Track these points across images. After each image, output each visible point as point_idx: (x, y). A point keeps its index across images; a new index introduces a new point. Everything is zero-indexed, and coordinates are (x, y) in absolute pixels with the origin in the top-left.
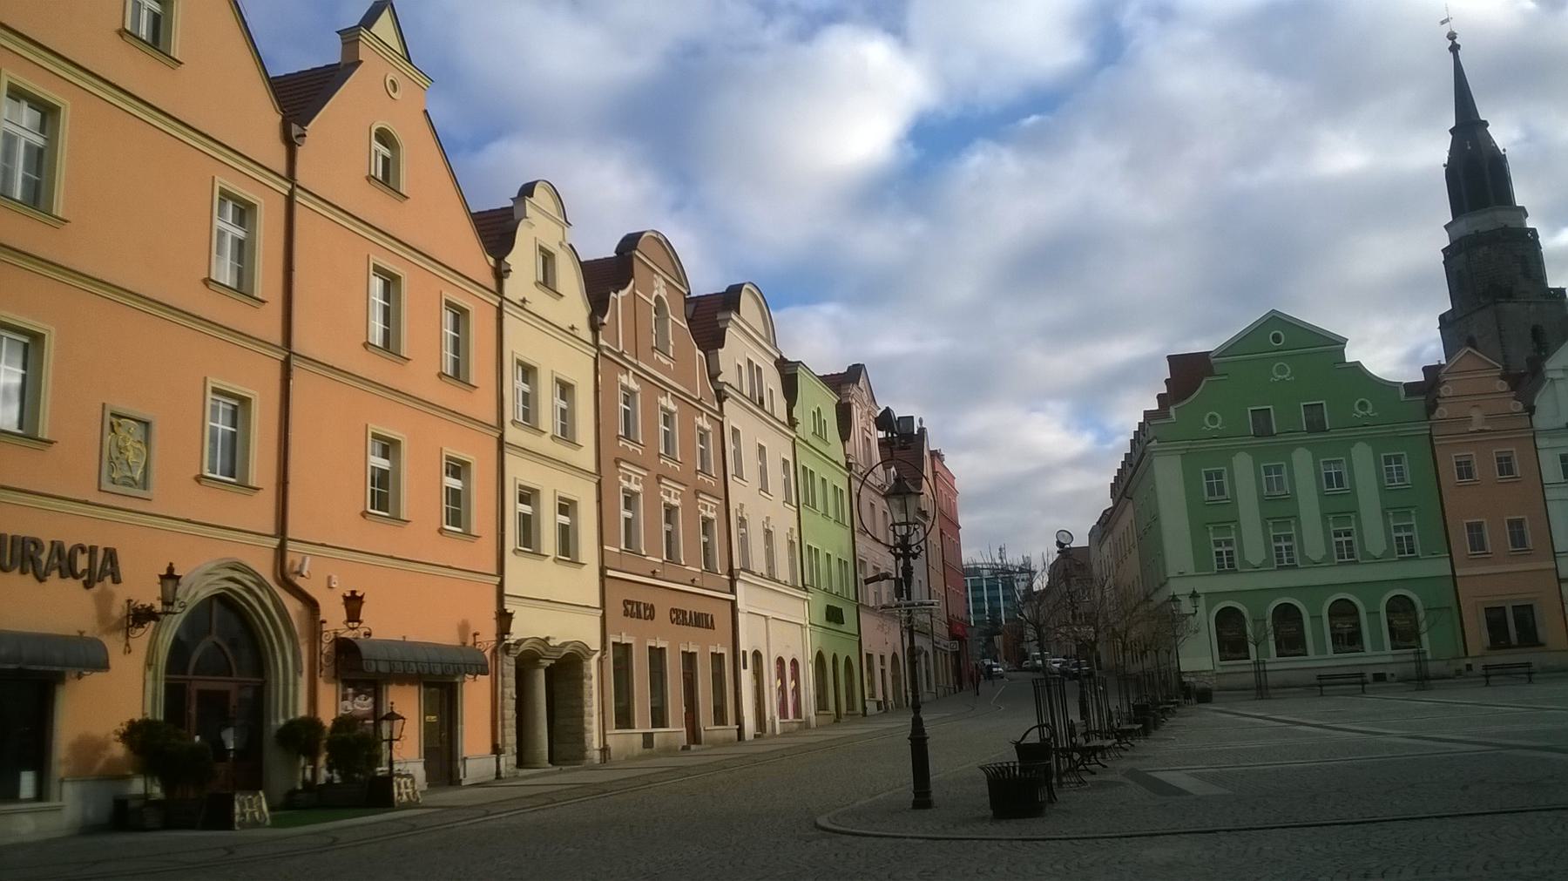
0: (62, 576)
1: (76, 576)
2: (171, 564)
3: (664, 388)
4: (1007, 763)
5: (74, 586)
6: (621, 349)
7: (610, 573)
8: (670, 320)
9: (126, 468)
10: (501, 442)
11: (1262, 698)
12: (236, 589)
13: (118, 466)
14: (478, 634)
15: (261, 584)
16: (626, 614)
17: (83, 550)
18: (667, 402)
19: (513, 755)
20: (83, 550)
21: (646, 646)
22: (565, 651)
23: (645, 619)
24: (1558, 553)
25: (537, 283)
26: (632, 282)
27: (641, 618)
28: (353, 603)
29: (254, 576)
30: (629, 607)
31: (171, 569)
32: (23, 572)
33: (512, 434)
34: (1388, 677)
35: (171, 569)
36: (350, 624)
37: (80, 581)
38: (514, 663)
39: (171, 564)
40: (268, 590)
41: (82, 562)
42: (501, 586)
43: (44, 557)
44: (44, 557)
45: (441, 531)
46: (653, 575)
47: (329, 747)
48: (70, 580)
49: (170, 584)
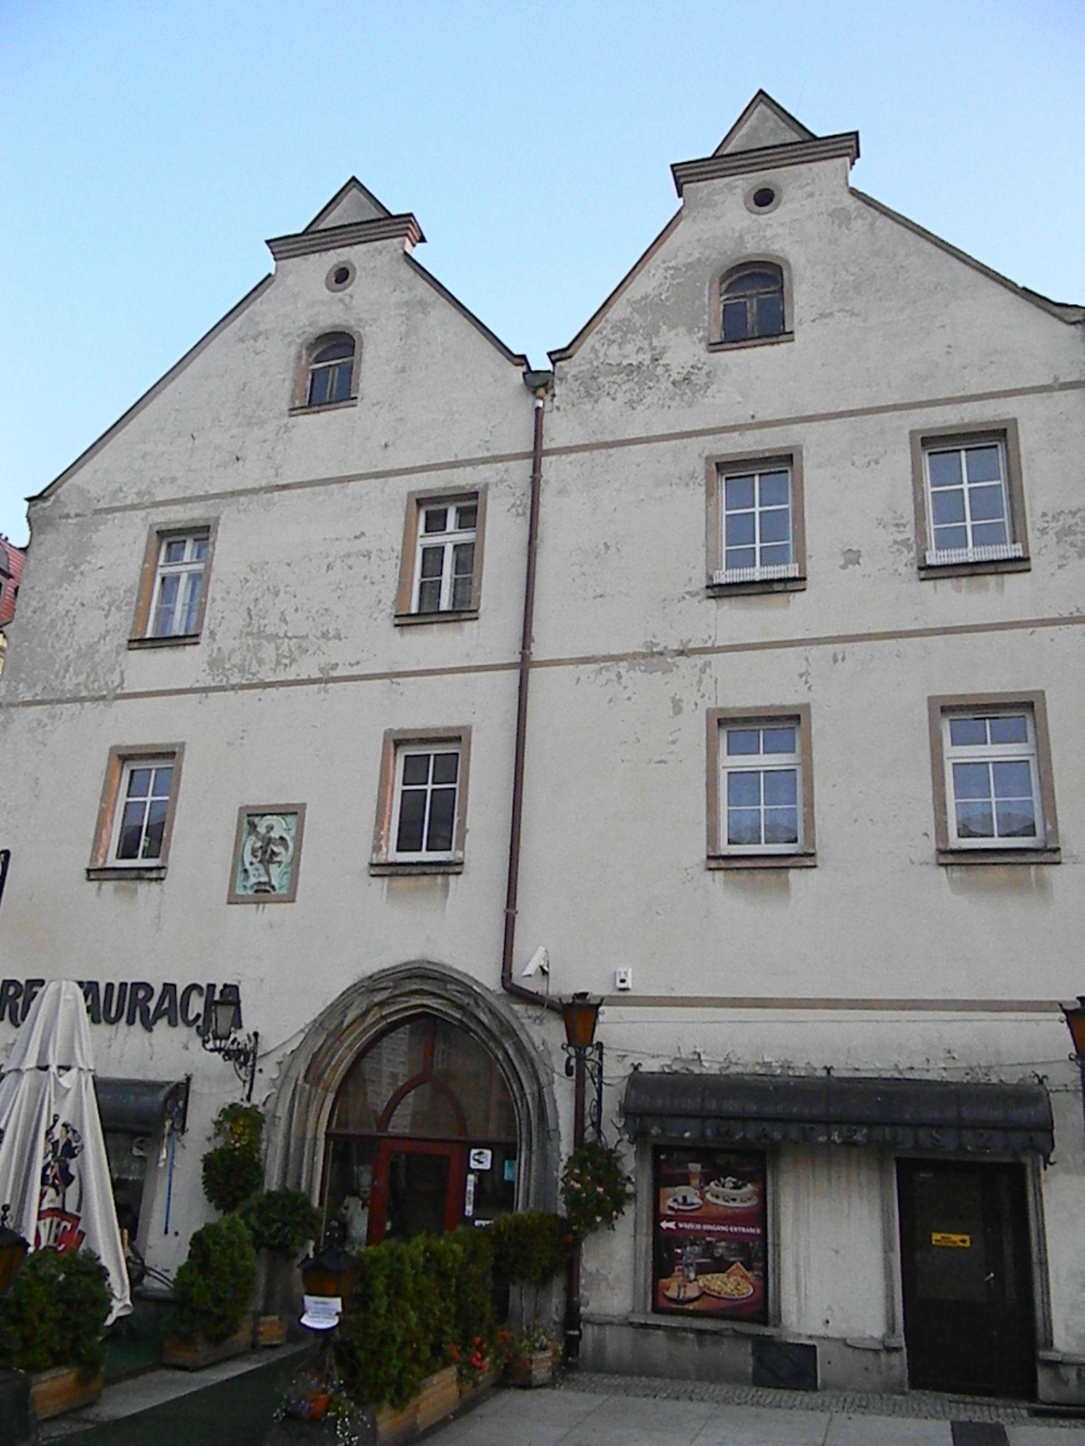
1: (189, 1024)
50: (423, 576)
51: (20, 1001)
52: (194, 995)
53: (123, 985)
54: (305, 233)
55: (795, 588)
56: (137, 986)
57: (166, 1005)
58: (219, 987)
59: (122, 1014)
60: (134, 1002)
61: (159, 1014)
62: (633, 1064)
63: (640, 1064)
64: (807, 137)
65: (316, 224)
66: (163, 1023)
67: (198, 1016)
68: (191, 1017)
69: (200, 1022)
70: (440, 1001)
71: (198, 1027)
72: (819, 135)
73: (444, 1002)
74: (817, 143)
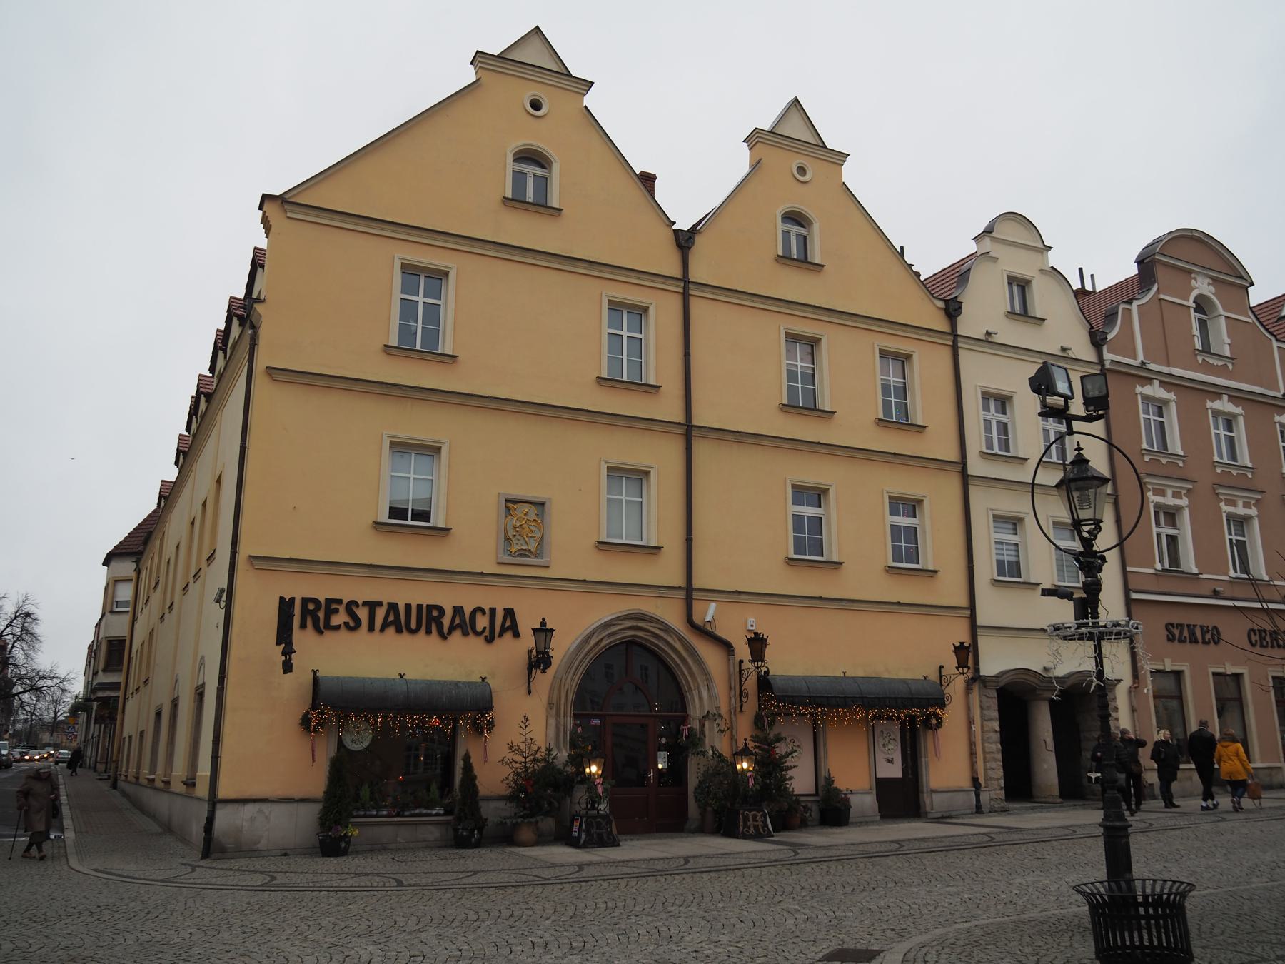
0: (962, 643)
1: (477, 634)
2: (544, 619)
3: (1216, 392)
4: (1237, 808)
5: (476, 643)
6: (1141, 357)
7: (1135, 596)
8: (1222, 320)
9: (522, 541)
10: (965, 478)
11: (928, 699)
12: (643, 636)
13: (515, 542)
14: (943, 667)
15: (667, 629)
16: (1171, 639)
17: (483, 612)
18: (1224, 405)
19: (1001, 789)
20: (483, 611)
21: (1208, 673)
22: (1069, 682)
23: (1204, 642)
24: (1254, 307)
25: (1011, 314)
26: (1155, 287)
27: (1196, 642)
28: (757, 644)
29: (662, 625)
30: (1177, 632)
31: (543, 623)
32: (429, 632)
33: (976, 466)
34: (119, 628)
35: (543, 623)
36: (961, 670)
37: (482, 637)
38: (995, 695)
39: (544, 619)
40: (676, 636)
41: (482, 622)
42: (973, 617)
43: (446, 621)
44: (446, 621)
45: (890, 570)
46: (1216, 594)
47: (1133, 787)
48: (472, 637)
49: (542, 635)
50: (1065, 581)
51: (321, 615)
52: (479, 617)
53: (420, 607)
54: (499, 57)
55: (572, 270)
56: (430, 608)
57: (391, 618)
58: (425, 606)
59: (421, 626)
60: (430, 619)
61: (452, 628)
62: (400, 674)
63: (404, 674)
64: (821, 145)
65: (505, 53)
66: (457, 634)
67: (485, 628)
68: (479, 629)
69: (487, 633)
70: (646, 633)
71: (486, 637)
72: (828, 147)
73: (649, 634)
74: (826, 150)
